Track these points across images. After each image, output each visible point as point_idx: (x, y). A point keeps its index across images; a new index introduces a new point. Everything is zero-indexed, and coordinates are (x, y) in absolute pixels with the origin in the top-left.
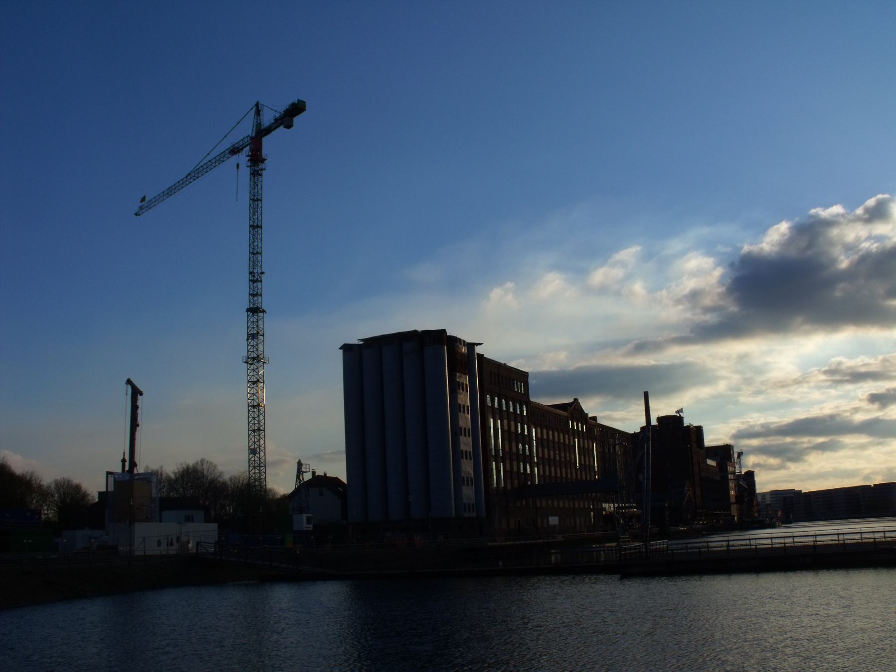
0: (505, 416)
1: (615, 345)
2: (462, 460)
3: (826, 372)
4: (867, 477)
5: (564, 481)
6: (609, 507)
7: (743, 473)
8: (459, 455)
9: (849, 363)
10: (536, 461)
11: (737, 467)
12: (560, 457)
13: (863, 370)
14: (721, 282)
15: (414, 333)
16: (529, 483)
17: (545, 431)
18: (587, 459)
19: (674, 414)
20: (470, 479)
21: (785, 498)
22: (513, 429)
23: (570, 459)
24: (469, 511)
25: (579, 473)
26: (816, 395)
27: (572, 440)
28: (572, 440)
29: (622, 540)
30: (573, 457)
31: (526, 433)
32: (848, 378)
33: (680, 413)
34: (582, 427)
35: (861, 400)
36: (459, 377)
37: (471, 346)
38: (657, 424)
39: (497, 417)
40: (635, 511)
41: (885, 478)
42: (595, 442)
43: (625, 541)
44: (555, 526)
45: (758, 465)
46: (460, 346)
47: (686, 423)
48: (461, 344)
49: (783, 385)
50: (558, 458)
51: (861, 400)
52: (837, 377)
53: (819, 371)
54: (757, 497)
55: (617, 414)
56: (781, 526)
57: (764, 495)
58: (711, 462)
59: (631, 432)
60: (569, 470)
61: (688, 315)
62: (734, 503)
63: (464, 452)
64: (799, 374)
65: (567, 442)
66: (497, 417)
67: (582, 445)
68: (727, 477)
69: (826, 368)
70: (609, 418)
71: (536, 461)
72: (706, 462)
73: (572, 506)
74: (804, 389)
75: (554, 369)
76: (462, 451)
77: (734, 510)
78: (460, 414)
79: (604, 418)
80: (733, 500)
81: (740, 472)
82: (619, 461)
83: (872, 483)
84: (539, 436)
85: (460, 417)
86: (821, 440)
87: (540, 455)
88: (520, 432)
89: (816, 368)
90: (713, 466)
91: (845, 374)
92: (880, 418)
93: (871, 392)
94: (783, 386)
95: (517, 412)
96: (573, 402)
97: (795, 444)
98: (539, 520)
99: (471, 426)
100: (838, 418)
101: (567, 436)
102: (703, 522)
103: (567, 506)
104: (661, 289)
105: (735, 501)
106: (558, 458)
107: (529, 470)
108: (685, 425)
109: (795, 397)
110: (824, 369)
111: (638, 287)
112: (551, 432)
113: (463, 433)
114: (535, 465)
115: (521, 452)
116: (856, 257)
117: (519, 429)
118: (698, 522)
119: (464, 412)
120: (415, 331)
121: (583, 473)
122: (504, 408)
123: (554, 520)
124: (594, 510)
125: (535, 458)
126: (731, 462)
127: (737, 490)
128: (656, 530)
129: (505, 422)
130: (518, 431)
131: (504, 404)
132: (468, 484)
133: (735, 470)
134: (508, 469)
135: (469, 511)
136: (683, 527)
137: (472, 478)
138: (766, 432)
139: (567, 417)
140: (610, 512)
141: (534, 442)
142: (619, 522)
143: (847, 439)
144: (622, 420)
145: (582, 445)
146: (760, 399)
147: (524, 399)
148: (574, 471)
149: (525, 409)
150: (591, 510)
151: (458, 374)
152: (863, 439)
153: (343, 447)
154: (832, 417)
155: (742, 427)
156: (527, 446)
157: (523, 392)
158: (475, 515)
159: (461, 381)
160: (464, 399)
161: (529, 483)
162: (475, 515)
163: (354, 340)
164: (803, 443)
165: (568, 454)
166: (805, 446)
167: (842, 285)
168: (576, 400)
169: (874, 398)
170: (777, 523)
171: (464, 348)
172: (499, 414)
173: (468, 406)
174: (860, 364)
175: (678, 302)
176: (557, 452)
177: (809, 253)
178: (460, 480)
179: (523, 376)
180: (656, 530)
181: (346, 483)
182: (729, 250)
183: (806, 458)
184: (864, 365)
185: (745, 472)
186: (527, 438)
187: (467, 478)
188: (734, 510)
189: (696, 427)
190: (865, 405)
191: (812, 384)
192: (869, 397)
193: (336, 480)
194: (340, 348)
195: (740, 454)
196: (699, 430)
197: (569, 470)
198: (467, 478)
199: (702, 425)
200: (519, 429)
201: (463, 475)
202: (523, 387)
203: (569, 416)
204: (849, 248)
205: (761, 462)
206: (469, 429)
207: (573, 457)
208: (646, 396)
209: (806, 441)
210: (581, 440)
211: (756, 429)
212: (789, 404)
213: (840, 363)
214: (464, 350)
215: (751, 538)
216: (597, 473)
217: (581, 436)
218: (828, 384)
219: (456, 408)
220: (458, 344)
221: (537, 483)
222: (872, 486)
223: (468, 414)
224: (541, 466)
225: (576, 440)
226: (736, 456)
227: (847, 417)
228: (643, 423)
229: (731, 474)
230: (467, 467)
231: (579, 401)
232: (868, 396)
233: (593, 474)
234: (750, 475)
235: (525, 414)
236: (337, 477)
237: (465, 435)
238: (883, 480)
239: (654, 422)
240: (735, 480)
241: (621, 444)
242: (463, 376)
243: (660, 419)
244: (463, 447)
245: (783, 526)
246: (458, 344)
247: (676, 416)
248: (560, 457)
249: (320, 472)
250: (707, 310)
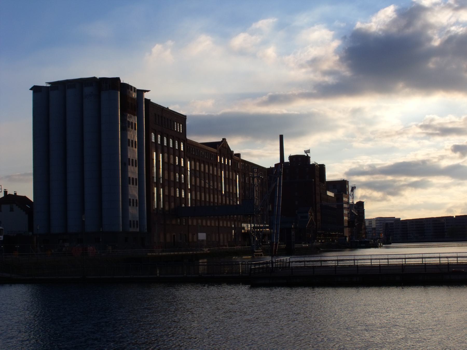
0: (166, 150)
1: (253, 96)
2: (129, 185)
3: (421, 127)
4: (449, 210)
5: (203, 205)
6: (247, 227)
7: (355, 203)
8: (126, 180)
9: (439, 120)
10: (189, 188)
11: (350, 198)
12: (209, 185)
13: (450, 126)
14: (336, 52)
15: (93, 80)
16: (183, 205)
17: (198, 164)
18: (231, 188)
19: (303, 154)
20: (135, 201)
21: (387, 224)
22: (172, 161)
23: (217, 188)
24: (134, 227)
25: (224, 198)
26: (414, 144)
27: (219, 172)
28: (219, 172)
29: (256, 254)
30: (220, 185)
31: (182, 165)
32: (438, 132)
33: (308, 154)
34: (227, 162)
35: (446, 150)
36: (129, 117)
37: (141, 92)
38: (289, 161)
39: (159, 151)
40: (268, 230)
41: (463, 211)
42: (238, 174)
43: (258, 255)
44: (203, 241)
45: (364, 197)
46: (131, 92)
47: (312, 161)
48: (132, 90)
49: (387, 135)
50: (207, 186)
51: (446, 150)
52: (430, 131)
53: (416, 125)
54: (365, 222)
55: (255, 152)
56: (382, 246)
57: (370, 221)
58: (330, 194)
59: (267, 167)
60: (216, 196)
61: (312, 76)
62: (347, 227)
63: (131, 179)
64: (402, 127)
65: (215, 173)
66: (159, 151)
67: (227, 177)
68: (343, 205)
69: (422, 124)
70: (248, 154)
71: (189, 188)
72: (326, 193)
73: (217, 225)
74: (404, 138)
75: (204, 113)
76: (130, 178)
77: (347, 232)
78: (129, 147)
79: (245, 154)
80: (346, 224)
81: (353, 202)
82: (256, 191)
83: (454, 215)
84: (193, 168)
85: (128, 150)
86: (414, 179)
87: (193, 183)
88: (177, 164)
89: (415, 123)
90: (331, 197)
91: (436, 129)
92: (461, 164)
93: (455, 144)
94: (387, 136)
95: (175, 147)
96: (222, 141)
97: (394, 181)
98: (190, 235)
99: (138, 158)
100: (428, 163)
101: (215, 169)
102: (321, 241)
103: (213, 225)
104: (289, 54)
105: (347, 226)
106: (207, 186)
107: (183, 194)
108: (311, 163)
109: (397, 145)
110: (420, 124)
111: (271, 51)
112: (202, 165)
113: (131, 163)
114: (189, 191)
115: (178, 181)
116: (445, 37)
117: (177, 162)
118: (318, 241)
119: (132, 146)
120: (94, 78)
121: (228, 199)
122: (165, 144)
123: (202, 236)
124: (235, 229)
125: (189, 185)
126: (346, 194)
127: (349, 216)
128: (283, 246)
129: (166, 155)
130: (176, 163)
131: (159, 140)
132: (133, 205)
133: (349, 201)
134: (167, 193)
135: (134, 227)
136: (305, 243)
137: (137, 200)
138: (373, 171)
139: (217, 153)
140: (248, 231)
141: (189, 172)
142: (254, 239)
143: (434, 180)
144: (259, 156)
145: (227, 177)
146: (369, 145)
147: (182, 137)
148: (220, 197)
149: (182, 145)
150: (232, 229)
151: (128, 115)
152: (446, 180)
153: (31, 170)
154: (424, 162)
155: (354, 166)
156: (183, 176)
157: (181, 132)
158: (138, 230)
159: (131, 120)
160: (133, 135)
161: (183, 205)
162: (138, 230)
163: (43, 83)
164: (401, 181)
165: (216, 183)
166: (402, 183)
167: (434, 59)
168: (224, 140)
169: (456, 149)
170: (379, 244)
171: (134, 93)
172: (161, 149)
173: (135, 142)
174: (448, 121)
175: (302, 66)
176: (207, 181)
177: (410, 31)
178: (126, 202)
179: (182, 119)
180: (283, 246)
181: (33, 201)
182: (342, 25)
183: (403, 193)
184: (451, 122)
185: (357, 203)
186: (183, 169)
187: (133, 200)
188: (347, 232)
189: (320, 165)
190: (450, 153)
191: (410, 135)
192: (452, 148)
193: (24, 199)
194: (31, 89)
195: (353, 188)
196: (322, 168)
197: (216, 196)
198: (133, 200)
199: (324, 164)
200: (177, 162)
201: (129, 197)
202: (181, 127)
203: (218, 152)
204: (442, 29)
205: (368, 194)
206: (136, 160)
207: (220, 185)
208: (281, 138)
209: (403, 179)
210: (227, 172)
211: (365, 168)
212: (391, 150)
213: (432, 120)
214: (134, 95)
215: (458, 256)
216: (238, 199)
217: (227, 169)
218: (423, 136)
219: (126, 143)
220: (130, 90)
221: (189, 206)
222: (454, 217)
223: (136, 147)
224: (193, 193)
225: (223, 172)
226: (350, 190)
227: (435, 162)
228: (278, 161)
229: (345, 203)
230: (133, 191)
231: (227, 141)
232: (452, 146)
233: (235, 199)
234: (361, 205)
235: (182, 149)
236: (25, 196)
237: (133, 165)
238: (461, 213)
239: (286, 160)
240: (348, 208)
241: (258, 177)
242: (133, 116)
243: (291, 158)
244: (130, 175)
245: (384, 246)
246: (130, 90)
247: (304, 156)
248: (209, 185)
249: (11, 192)
250: (325, 73)
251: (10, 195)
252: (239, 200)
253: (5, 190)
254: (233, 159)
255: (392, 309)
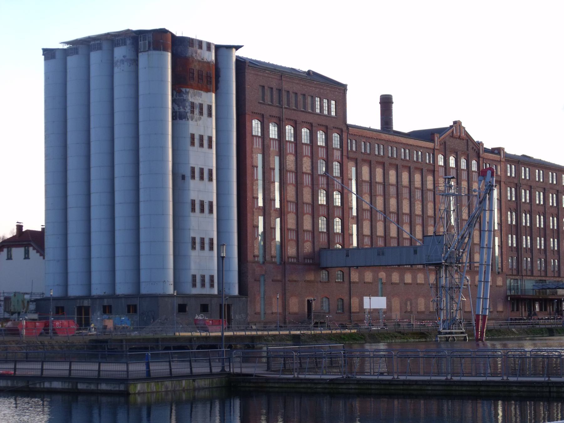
157: (333, 114)
163: (56, 44)
251: (29, 232)
252: (499, 234)
253: (18, 223)
254: (481, 159)
255: (119, 333)
